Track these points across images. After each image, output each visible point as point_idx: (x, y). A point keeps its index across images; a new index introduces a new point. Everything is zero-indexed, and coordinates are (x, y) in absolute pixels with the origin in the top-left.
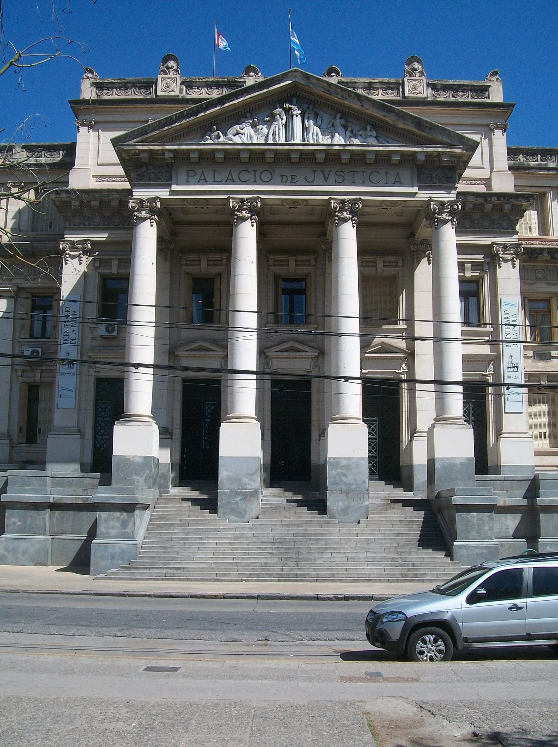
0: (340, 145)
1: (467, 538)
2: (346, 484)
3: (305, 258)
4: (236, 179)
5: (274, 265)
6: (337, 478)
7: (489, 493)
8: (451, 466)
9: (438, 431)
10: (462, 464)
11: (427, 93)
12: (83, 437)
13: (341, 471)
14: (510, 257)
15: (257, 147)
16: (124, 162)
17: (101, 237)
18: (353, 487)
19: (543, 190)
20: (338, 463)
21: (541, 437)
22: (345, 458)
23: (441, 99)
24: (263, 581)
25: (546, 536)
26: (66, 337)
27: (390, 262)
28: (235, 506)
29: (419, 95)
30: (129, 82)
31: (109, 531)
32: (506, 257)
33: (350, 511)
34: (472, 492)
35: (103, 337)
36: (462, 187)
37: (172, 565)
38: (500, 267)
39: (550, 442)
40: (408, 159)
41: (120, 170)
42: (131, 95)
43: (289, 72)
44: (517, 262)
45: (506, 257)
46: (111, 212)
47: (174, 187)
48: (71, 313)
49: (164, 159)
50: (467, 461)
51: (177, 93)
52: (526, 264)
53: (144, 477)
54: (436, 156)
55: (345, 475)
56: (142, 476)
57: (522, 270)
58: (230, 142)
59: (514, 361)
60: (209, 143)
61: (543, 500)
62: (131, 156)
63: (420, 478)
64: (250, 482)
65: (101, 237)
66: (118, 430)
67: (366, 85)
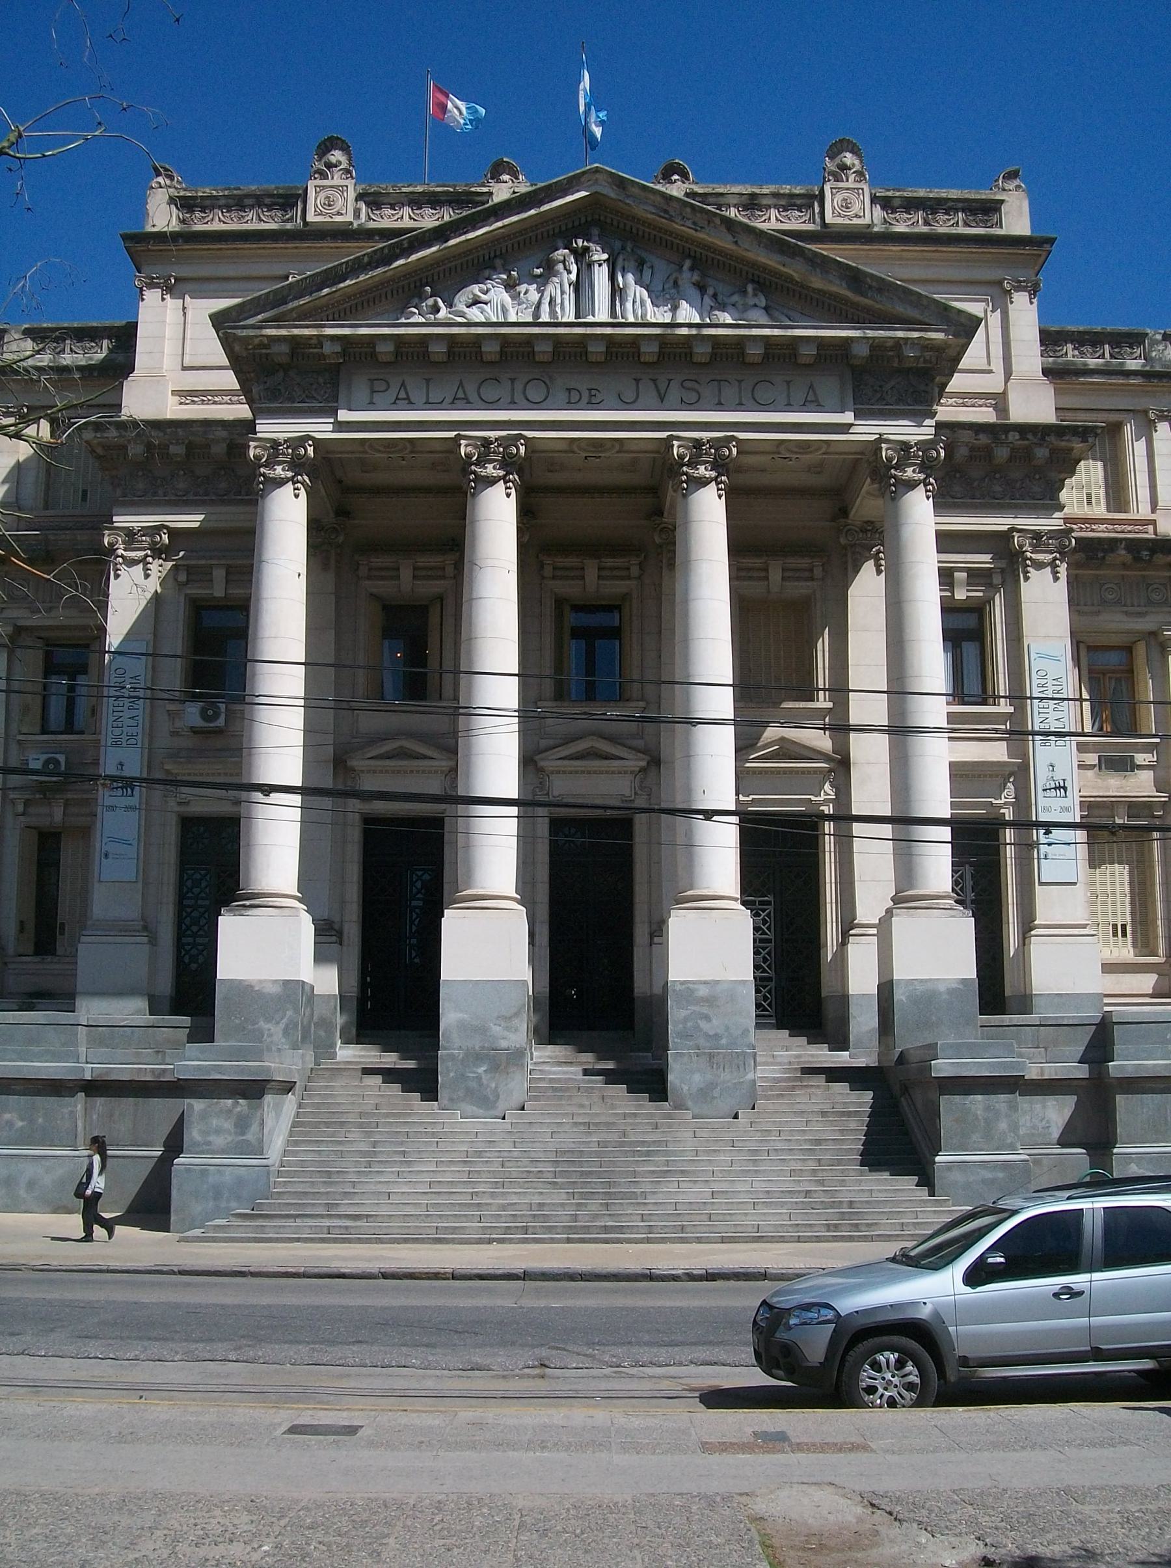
0: (690, 325)
1: (963, 1147)
4: (473, 396)
5: (554, 578)
6: (689, 1024)
8: (928, 997)
9: (901, 924)
10: (951, 992)
11: (873, 217)
16: (237, 363)
17: (190, 520)
18: (724, 1041)
20: (691, 992)
21: (1115, 934)
22: (705, 982)
23: (900, 228)
25: (1132, 1140)
28: (474, 1085)
29: (856, 221)
30: (247, 196)
31: (211, 1138)
32: (1040, 557)
34: (972, 1051)
35: (195, 731)
36: (946, 412)
37: (342, 1210)
38: (1027, 579)
39: (1134, 946)
40: (833, 355)
41: (229, 380)
43: (584, 173)
44: (1063, 568)
45: (1040, 557)
46: (211, 468)
47: (344, 415)
49: (322, 356)
50: (961, 987)
51: (349, 217)
53: (282, 1026)
54: (891, 349)
55: (707, 1018)
56: (278, 1023)
58: (460, 320)
60: (415, 322)
61: (1121, 1065)
62: (254, 348)
63: (863, 1021)
64: (506, 1033)
65: (190, 520)
66: (229, 926)
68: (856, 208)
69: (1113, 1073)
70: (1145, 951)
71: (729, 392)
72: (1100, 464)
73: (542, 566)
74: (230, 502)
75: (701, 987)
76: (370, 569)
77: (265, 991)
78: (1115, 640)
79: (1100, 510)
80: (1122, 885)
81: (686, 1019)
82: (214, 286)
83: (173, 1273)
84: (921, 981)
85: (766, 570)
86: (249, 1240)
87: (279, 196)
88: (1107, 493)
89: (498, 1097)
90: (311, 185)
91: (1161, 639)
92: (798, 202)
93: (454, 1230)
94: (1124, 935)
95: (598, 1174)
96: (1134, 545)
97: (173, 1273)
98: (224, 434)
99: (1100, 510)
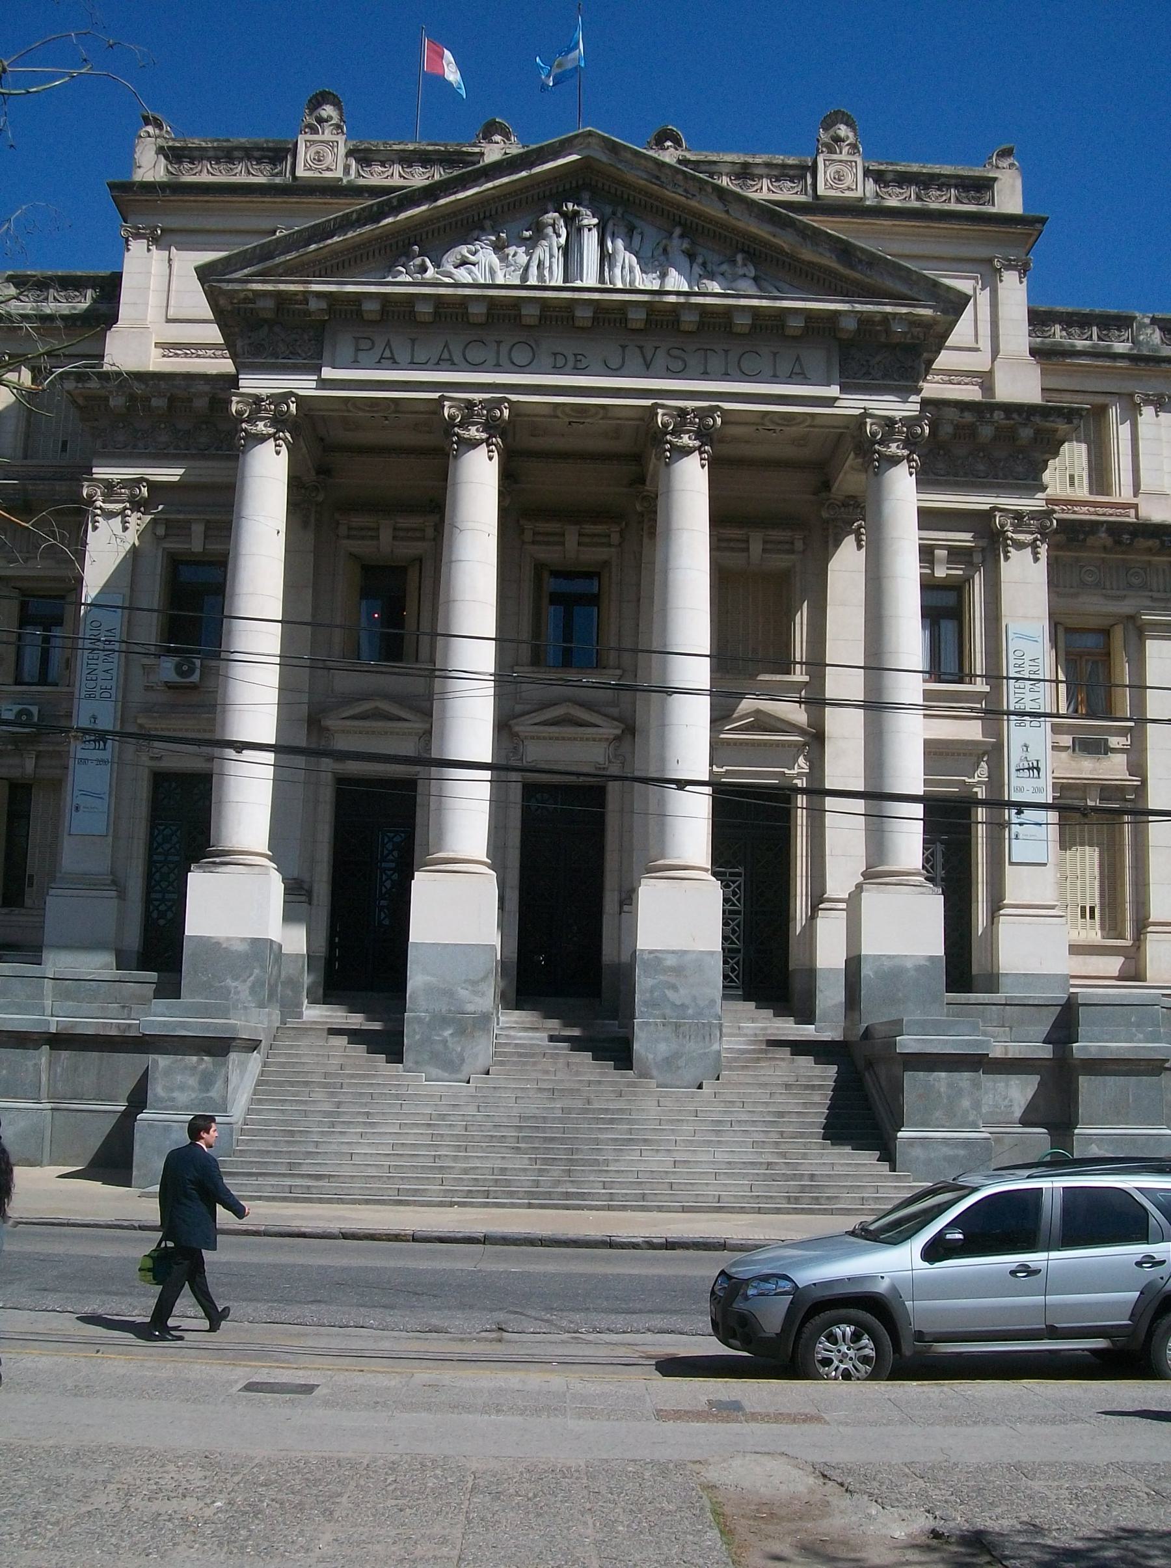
0: (678, 293)
1: (924, 1124)
2: (673, 1004)
3: (600, 528)
8: (895, 973)
9: (871, 899)
10: (918, 968)
12: (122, 895)
14: (1029, 538)
15: (503, 293)
16: (222, 317)
17: (171, 474)
18: (690, 1011)
19: (1100, 400)
20: (659, 960)
21: (1083, 916)
22: (673, 952)
23: (893, 202)
25: (1091, 1122)
26: (92, 684)
28: (440, 1047)
29: (848, 194)
30: (236, 148)
31: (175, 1095)
33: (681, 1062)
34: (938, 1028)
35: (170, 686)
39: (1102, 928)
40: (820, 328)
41: (213, 334)
42: (240, 175)
43: (576, 136)
44: (1043, 550)
46: (194, 422)
47: (328, 373)
48: (1027, 663)
49: (307, 313)
51: (339, 173)
52: (1061, 553)
53: (249, 984)
54: (881, 323)
55: (674, 988)
56: (245, 981)
58: (447, 280)
59: (1032, 756)
60: (402, 281)
61: (1085, 1047)
62: (239, 303)
63: (830, 996)
65: (171, 474)
66: (197, 881)
67: (737, 169)
68: (849, 180)
71: (715, 362)
72: (1084, 446)
73: (522, 531)
75: (670, 956)
76: (349, 529)
77: (234, 948)
79: (1082, 492)
80: (1092, 868)
82: (200, 238)
84: (889, 957)
87: (269, 149)
88: (1090, 476)
89: (463, 1060)
90: (301, 139)
91: (1139, 623)
92: (791, 173)
95: (562, 1141)
96: (1116, 529)
98: (207, 388)
99: (1082, 492)
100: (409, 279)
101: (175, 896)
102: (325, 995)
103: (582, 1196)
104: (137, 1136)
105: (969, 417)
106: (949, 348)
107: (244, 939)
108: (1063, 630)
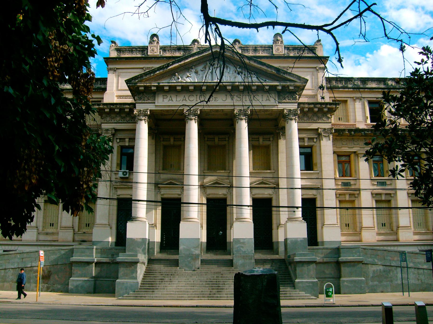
0: (239, 82)
1: (302, 278)
5: (208, 141)
7: (313, 255)
8: (295, 242)
9: (289, 225)
10: (301, 241)
12: (111, 228)
13: (240, 245)
15: (197, 84)
16: (130, 90)
20: (239, 241)
23: (292, 55)
24: (201, 299)
25: (345, 277)
27: (266, 138)
29: (281, 53)
34: (304, 255)
35: (121, 178)
36: (302, 100)
40: (273, 89)
41: (129, 93)
44: (331, 136)
46: (125, 112)
49: (151, 90)
51: (158, 54)
52: (337, 137)
54: (287, 87)
55: (243, 247)
57: (334, 140)
58: (184, 81)
60: (173, 81)
61: (342, 258)
63: (282, 248)
66: (129, 225)
67: (254, 48)
68: (281, 50)
69: (340, 260)
70: (354, 230)
73: (205, 138)
74: (130, 123)
78: (346, 154)
81: (238, 247)
83: (116, 306)
85: (259, 139)
86: (134, 299)
92: (267, 49)
93: (182, 297)
94: (421, 226)
95: (216, 284)
96: (350, 131)
97: (116, 306)
100: (175, 81)
101: (124, 228)
102: (160, 251)
103: (221, 297)
104: (116, 286)
105: (312, 106)
106: (306, 89)
107: (140, 238)
108: (338, 155)
